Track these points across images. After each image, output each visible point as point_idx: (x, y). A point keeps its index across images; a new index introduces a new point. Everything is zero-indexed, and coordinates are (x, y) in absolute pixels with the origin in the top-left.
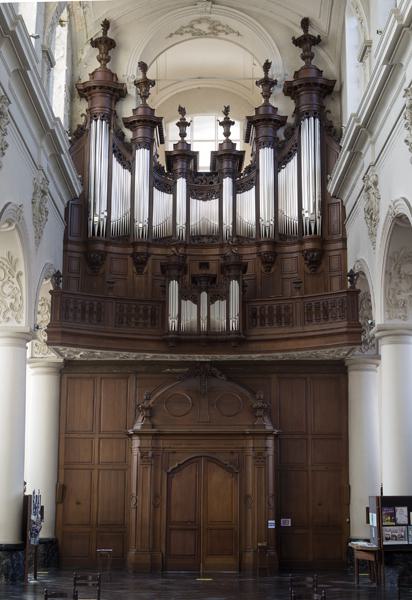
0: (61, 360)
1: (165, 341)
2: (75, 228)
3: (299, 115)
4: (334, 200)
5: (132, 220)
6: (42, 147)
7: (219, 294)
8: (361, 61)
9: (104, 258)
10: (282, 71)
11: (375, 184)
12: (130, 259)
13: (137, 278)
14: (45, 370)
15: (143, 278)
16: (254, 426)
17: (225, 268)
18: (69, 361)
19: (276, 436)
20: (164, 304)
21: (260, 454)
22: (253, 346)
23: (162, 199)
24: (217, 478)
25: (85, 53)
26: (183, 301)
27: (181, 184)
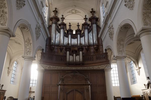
0: (44, 69)
1: (66, 64)
3: (92, 24)
4: (100, 38)
6: (39, 19)
7: (78, 54)
9: (54, 49)
10: (88, 17)
11: (112, 26)
13: (61, 53)
15: (62, 53)
16: (86, 83)
17: (79, 49)
19: (91, 85)
20: (66, 56)
21: (87, 89)
22: (85, 65)
23: (66, 39)
24: (78, 95)
25: (52, 14)
26: (70, 56)
27: (70, 36)
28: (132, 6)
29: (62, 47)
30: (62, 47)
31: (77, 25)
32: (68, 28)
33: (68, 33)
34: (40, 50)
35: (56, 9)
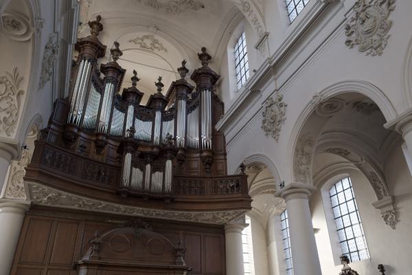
0: (29, 203)
1: (118, 194)
2: (58, 116)
3: (201, 88)
4: (219, 134)
5: (98, 120)
8: (267, 35)
9: (75, 139)
12: (93, 144)
14: (12, 209)
18: (36, 205)
23: (119, 115)
25: (83, 30)
26: (134, 169)
27: (131, 109)
28: (380, 46)
29: (104, 138)
30: (104, 138)
31: (158, 82)
32: (126, 84)
33: (124, 100)
34: (34, 132)
35: (99, 18)
